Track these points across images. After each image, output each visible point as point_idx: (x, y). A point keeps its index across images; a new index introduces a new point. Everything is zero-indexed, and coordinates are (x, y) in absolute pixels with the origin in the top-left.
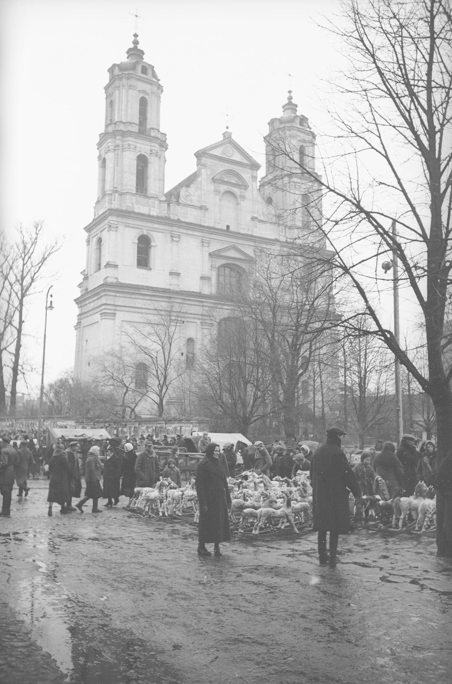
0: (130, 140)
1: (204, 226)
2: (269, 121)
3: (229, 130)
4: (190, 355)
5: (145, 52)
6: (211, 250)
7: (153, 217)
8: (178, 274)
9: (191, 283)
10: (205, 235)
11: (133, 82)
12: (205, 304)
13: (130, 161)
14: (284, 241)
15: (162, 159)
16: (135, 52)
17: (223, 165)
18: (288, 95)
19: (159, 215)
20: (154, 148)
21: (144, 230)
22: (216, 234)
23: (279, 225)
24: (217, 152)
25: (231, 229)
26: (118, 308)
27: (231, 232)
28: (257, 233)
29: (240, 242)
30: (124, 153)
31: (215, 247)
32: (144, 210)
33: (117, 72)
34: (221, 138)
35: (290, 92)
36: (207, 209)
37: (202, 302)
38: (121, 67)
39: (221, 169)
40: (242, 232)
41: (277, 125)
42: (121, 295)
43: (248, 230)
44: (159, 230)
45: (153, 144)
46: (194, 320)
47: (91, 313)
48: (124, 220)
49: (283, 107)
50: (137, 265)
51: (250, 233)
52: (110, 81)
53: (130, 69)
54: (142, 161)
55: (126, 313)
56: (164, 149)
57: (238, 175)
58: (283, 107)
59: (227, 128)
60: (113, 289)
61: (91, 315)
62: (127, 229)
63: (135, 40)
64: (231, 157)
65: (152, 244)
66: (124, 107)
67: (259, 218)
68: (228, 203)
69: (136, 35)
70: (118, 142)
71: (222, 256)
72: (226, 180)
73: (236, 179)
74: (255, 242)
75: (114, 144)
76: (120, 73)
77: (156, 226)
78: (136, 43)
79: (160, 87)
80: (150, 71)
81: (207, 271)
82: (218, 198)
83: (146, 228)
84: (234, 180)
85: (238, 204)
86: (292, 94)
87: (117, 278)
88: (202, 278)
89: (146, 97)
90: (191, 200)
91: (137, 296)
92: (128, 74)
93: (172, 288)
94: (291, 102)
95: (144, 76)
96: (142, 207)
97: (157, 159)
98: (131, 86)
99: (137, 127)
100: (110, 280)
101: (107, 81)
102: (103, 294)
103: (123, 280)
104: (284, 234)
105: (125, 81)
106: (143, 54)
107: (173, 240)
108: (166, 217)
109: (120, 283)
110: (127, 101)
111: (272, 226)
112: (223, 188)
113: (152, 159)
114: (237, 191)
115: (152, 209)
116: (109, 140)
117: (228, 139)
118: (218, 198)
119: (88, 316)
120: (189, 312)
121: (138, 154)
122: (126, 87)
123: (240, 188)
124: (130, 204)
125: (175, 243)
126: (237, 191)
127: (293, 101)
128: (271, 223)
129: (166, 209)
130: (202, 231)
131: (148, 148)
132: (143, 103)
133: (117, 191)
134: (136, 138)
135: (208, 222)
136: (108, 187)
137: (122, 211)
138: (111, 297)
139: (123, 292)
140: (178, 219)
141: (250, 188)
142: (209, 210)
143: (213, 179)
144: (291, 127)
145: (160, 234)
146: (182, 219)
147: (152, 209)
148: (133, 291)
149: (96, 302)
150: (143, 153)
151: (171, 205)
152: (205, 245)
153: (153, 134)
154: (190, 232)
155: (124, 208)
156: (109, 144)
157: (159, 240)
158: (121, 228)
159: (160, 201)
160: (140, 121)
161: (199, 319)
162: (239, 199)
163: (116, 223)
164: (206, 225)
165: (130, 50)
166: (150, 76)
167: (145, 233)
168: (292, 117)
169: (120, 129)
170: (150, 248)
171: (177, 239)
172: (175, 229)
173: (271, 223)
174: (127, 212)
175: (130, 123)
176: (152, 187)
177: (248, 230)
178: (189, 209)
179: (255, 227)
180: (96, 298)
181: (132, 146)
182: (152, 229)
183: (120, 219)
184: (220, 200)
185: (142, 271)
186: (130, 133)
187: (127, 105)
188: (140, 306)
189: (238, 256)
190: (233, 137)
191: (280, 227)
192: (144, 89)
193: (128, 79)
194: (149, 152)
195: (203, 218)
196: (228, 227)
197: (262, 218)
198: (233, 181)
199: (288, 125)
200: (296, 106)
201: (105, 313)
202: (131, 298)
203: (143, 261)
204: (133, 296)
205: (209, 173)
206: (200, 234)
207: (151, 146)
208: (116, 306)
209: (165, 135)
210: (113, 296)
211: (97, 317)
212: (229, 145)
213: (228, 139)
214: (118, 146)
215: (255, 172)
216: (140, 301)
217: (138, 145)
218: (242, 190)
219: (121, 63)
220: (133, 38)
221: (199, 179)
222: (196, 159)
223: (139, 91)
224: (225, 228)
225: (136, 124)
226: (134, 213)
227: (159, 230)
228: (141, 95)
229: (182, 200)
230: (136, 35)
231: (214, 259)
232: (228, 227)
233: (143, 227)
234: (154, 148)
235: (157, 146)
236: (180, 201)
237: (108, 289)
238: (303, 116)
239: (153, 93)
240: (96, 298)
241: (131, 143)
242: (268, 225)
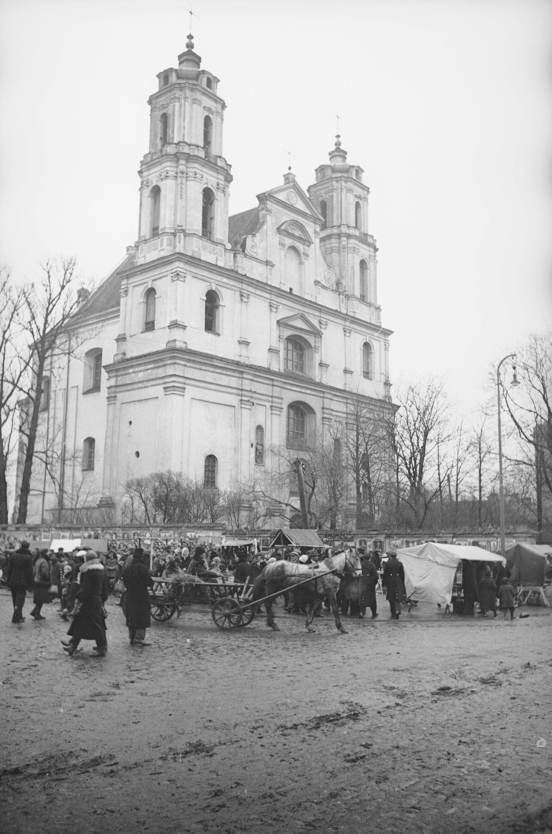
0: (196, 167)
2: (318, 167)
4: (259, 447)
6: (279, 318)
8: (247, 344)
9: (259, 357)
10: (273, 297)
12: (275, 383)
14: (345, 312)
16: (190, 56)
18: (336, 140)
21: (213, 284)
23: (340, 294)
26: (188, 381)
29: (311, 311)
30: (188, 183)
31: (283, 313)
35: (338, 136)
37: (273, 380)
40: (306, 297)
42: (191, 365)
46: (264, 403)
47: (140, 385)
49: (330, 154)
50: (206, 328)
53: (192, 79)
55: (196, 389)
57: (302, 228)
59: (290, 168)
60: (184, 357)
61: (139, 388)
62: (194, 280)
68: (291, 260)
69: (190, 37)
73: (300, 233)
74: (320, 312)
75: (175, 169)
77: (225, 280)
81: (275, 344)
83: (215, 281)
84: (297, 233)
86: (340, 139)
87: (185, 343)
88: (270, 350)
89: (211, 116)
91: (208, 368)
92: (194, 84)
93: (242, 360)
96: (208, 254)
98: (195, 99)
100: (179, 345)
102: (169, 362)
103: (192, 346)
107: (241, 299)
110: (191, 118)
112: (288, 242)
113: (218, 195)
114: (300, 247)
116: (168, 164)
119: (134, 389)
120: (258, 392)
121: (205, 186)
122: (189, 100)
123: (304, 244)
124: (197, 250)
125: (244, 305)
126: (300, 247)
127: (342, 147)
128: (333, 290)
129: (232, 260)
132: (208, 122)
134: (203, 166)
138: (180, 367)
139: (194, 362)
140: (245, 275)
143: (278, 229)
148: (205, 361)
149: (149, 371)
150: (210, 186)
151: (238, 256)
156: (168, 168)
157: (228, 298)
158: (189, 278)
161: (268, 401)
162: (302, 256)
163: (184, 271)
167: (214, 289)
170: (217, 307)
180: (152, 366)
181: (198, 176)
182: (220, 284)
183: (188, 267)
185: (210, 336)
188: (209, 380)
189: (305, 327)
193: (192, 90)
194: (215, 186)
196: (291, 289)
198: (297, 234)
200: (346, 153)
201: (174, 386)
202: (201, 369)
204: (203, 368)
207: (218, 178)
208: (187, 378)
209: (230, 166)
210: (171, 364)
211: (158, 391)
212: (292, 190)
216: (210, 374)
217: (205, 176)
218: (306, 247)
221: (264, 228)
223: (204, 107)
228: (206, 113)
229: (248, 250)
230: (190, 37)
231: (281, 328)
232: (291, 289)
233: (211, 281)
236: (246, 252)
238: (358, 167)
240: (152, 366)
241: (198, 171)
242: (330, 292)
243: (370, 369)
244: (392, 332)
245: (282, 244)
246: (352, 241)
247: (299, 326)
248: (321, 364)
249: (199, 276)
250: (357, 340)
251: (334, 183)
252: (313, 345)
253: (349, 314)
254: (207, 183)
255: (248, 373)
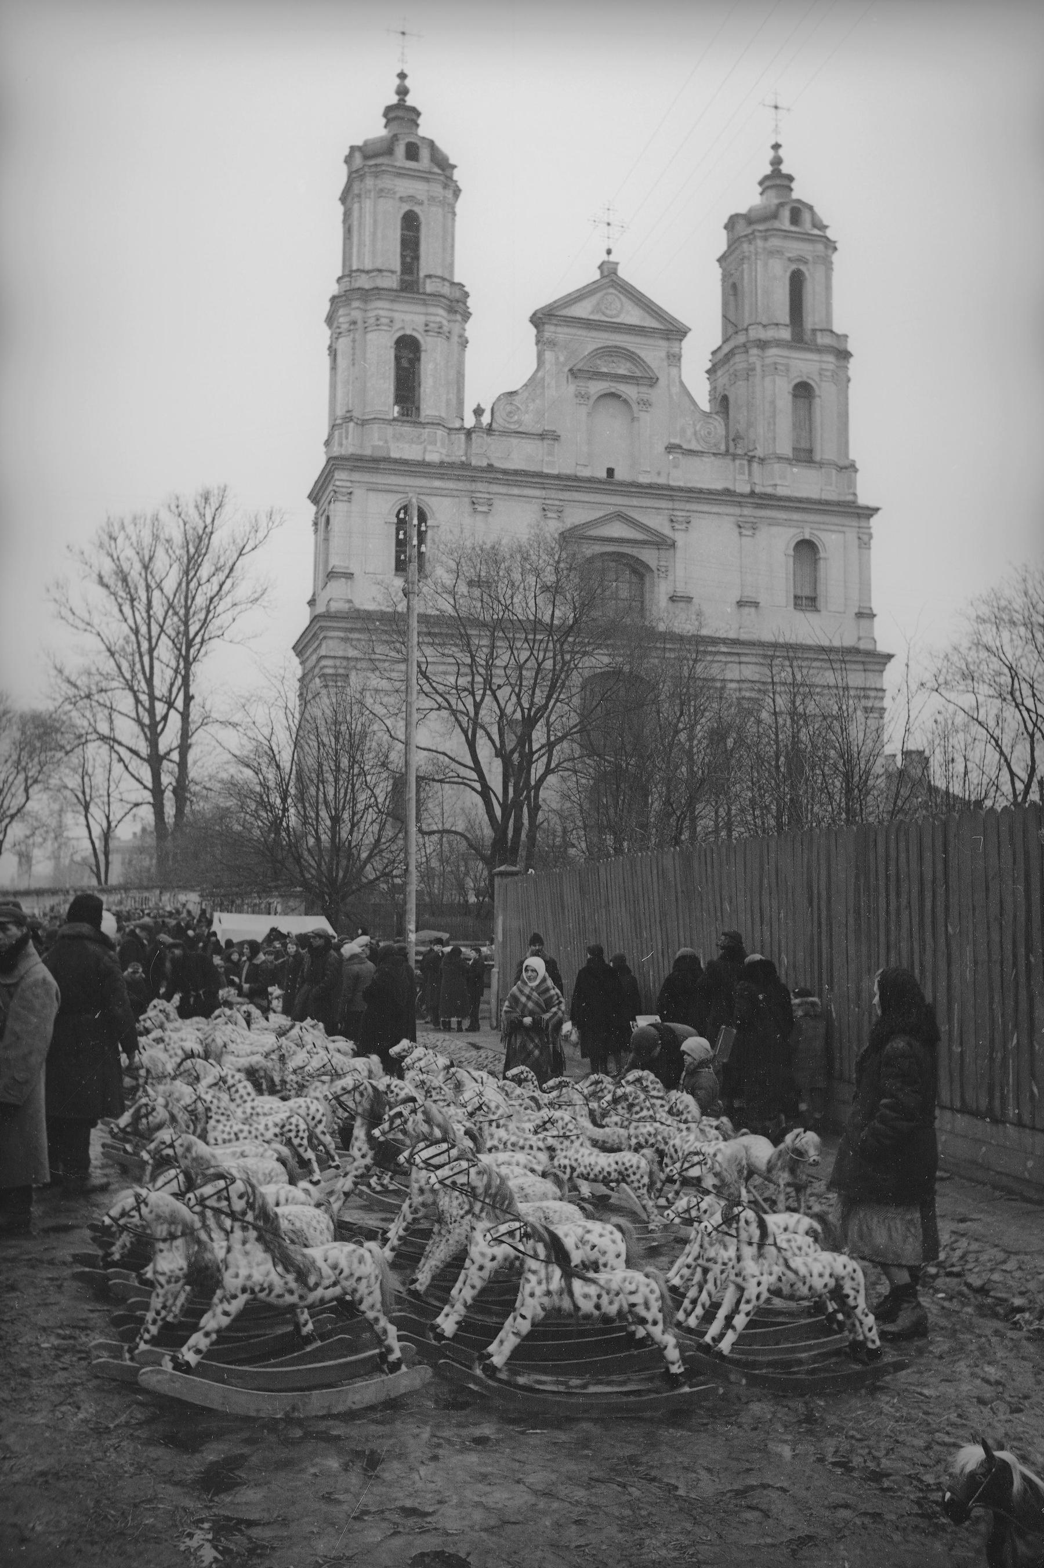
0: (380, 308)
1: (548, 476)
2: (725, 220)
3: (612, 258)
5: (419, 108)
7: (429, 465)
10: (553, 494)
11: (387, 182)
13: (380, 350)
15: (455, 339)
17: (603, 335)
19: (447, 459)
20: (432, 318)
22: (698, 500)
23: (735, 457)
24: (582, 310)
25: (619, 475)
27: (622, 484)
28: (678, 479)
29: (635, 502)
30: (369, 336)
32: (410, 452)
33: (742, 229)
34: (596, 275)
35: (776, 147)
36: (556, 438)
38: (749, 219)
39: (591, 347)
40: (644, 479)
41: (742, 229)
43: (659, 474)
44: (444, 492)
45: (432, 310)
48: (367, 477)
49: (761, 183)
51: (661, 480)
52: (729, 247)
54: (408, 350)
56: (459, 317)
57: (632, 357)
58: (761, 183)
59: (609, 252)
62: (371, 494)
63: (399, 87)
64: (617, 316)
65: (822, 555)
66: (367, 240)
67: (685, 446)
68: (611, 424)
69: (402, 76)
70: (357, 315)
71: (590, 538)
72: (605, 370)
73: (629, 365)
76: (749, 230)
77: (437, 483)
78: (403, 92)
79: (831, 246)
80: (806, 216)
82: (584, 411)
83: (808, 527)
85: (633, 419)
86: (781, 152)
87: (350, 601)
89: (417, 209)
90: (519, 422)
94: (779, 171)
95: (793, 228)
96: (407, 446)
97: (440, 341)
98: (382, 190)
99: (789, 329)
101: (722, 247)
104: (746, 477)
105: (369, 182)
106: (419, 114)
108: (463, 463)
109: (358, 611)
111: (718, 462)
112: (597, 387)
115: (429, 448)
117: (609, 273)
118: (584, 411)
124: (381, 443)
125: (479, 518)
127: (785, 169)
128: (714, 454)
130: (671, 498)
131: (420, 320)
133: (351, 419)
134: (393, 301)
135: (561, 463)
136: (340, 412)
137: (360, 458)
140: (490, 466)
141: (663, 382)
142: (562, 438)
143: (571, 370)
144: (767, 230)
145: (447, 502)
146: (497, 464)
147: (429, 448)
150: (408, 332)
152: (550, 515)
153: (822, 340)
154: (516, 491)
155: (368, 452)
159: (450, 429)
160: (403, 263)
162: (635, 406)
164: (555, 472)
165: (389, 110)
166: (425, 161)
168: (773, 207)
169: (357, 285)
171: (485, 509)
172: (480, 486)
173: (714, 454)
174: (375, 460)
175: (380, 271)
176: (432, 399)
177: (659, 474)
178: (514, 441)
179: (676, 467)
181: (383, 320)
183: (356, 476)
184: (589, 414)
186: (779, 343)
187: (374, 234)
190: (623, 273)
191: (738, 462)
192: (411, 192)
193: (376, 175)
194: (421, 328)
195: (546, 459)
196: (610, 472)
197: (694, 446)
199: (761, 227)
200: (790, 178)
203: (807, 602)
205: (562, 359)
206: (537, 493)
212: (612, 290)
213: (609, 273)
214: (354, 323)
215: (676, 344)
217: (396, 315)
218: (643, 389)
219: (366, 143)
220: (771, 153)
222: (534, 331)
223: (401, 198)
224: (603, 475)
225: (393, 272)
226: (387, 460)
227: (444, 492)
228: (406, 208)
230: (402, 76)
232: (610, 472)
234: (432, 318)
235: (441, 312)
237: (329, 624)
239: (432, 199)
241: (381, 313)
242: (708, 460)
243: (821, 588)
244: (877, 510)
245: (582, 396)
246: (773, 351)
247: (616, 535)
248: (672, 599)
249: (380, 487)
250: (777, 541)
251: (745, 246)
252: (653, 564)
253: (757, 490)
254: (403, 328)
255: (334, 629)
